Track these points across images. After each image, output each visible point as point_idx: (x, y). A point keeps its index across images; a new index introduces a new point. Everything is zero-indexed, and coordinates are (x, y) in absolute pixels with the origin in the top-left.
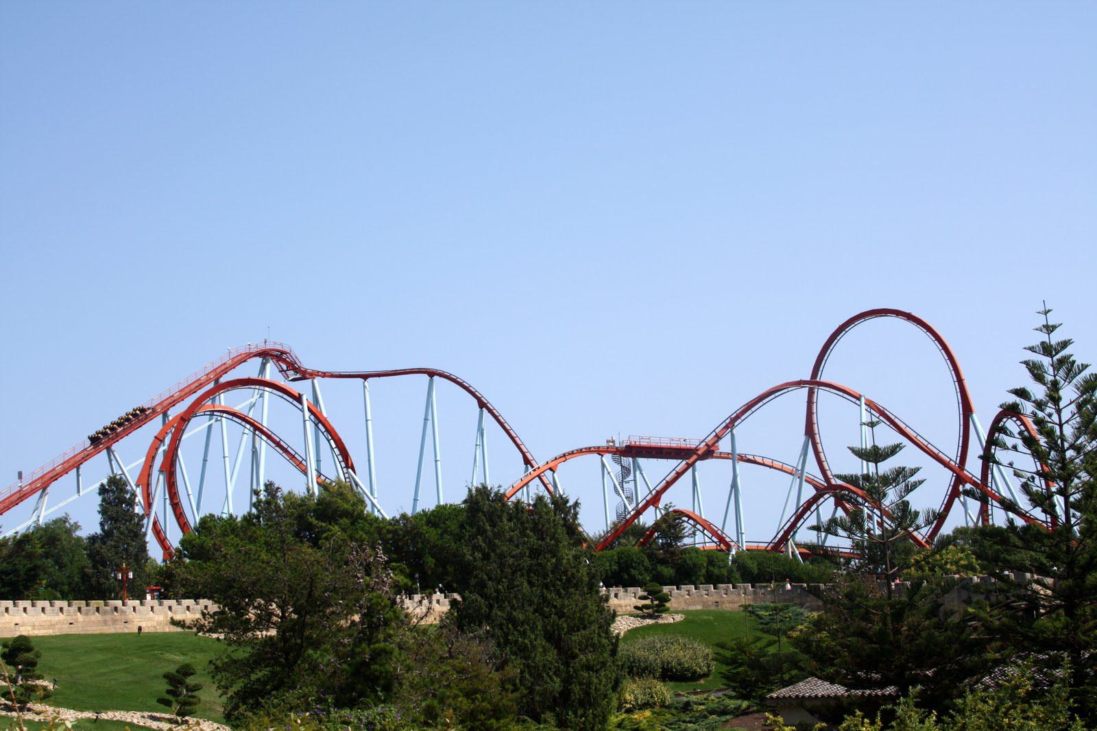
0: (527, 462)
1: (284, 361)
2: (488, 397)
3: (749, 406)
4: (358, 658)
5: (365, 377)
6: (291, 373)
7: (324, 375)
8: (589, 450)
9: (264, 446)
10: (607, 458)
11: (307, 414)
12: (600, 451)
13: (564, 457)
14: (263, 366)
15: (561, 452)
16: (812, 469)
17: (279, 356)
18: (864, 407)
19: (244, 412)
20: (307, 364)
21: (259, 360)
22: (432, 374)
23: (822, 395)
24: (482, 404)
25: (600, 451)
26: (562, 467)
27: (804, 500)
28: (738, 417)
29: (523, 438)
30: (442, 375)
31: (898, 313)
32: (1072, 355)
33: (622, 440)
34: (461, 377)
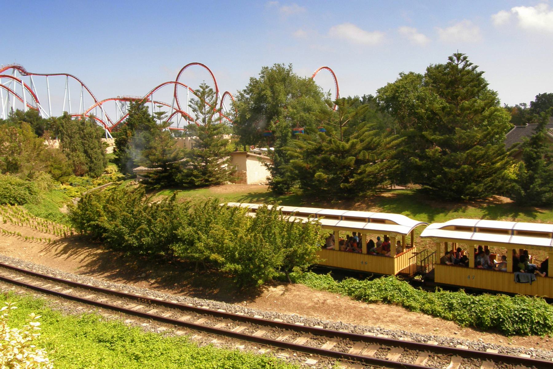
0: (96, 102)
1: (21, 70)
2: (84, 83)
3: (157, 88)
4: (226, 137)
5: (47, 75)
6: (23, 73)
7: (34, 74)
8: (112, 99)
9: (10, 93)
10: (117, 101)
11: (23, 86)
12: (115, 99)
13: (105, 101)
14: (14, 72)
15: (103, 99)
16: (176, 106)
17: (19, 68)
18: (188, 89)
19: (7, 86)
20: (28, 71)
21: (12, 69)
22: (67, 75)
23: (178, 86)
24: (83, 85)
25: (115, 99)
26: (104, 103)
27: (173, 112)
28: (153, 91)
29: (94, 95)
30: (70, 76)
31: (200, 64)
32: (483, 72)
33: (121, 96)
34: (76, 77)
